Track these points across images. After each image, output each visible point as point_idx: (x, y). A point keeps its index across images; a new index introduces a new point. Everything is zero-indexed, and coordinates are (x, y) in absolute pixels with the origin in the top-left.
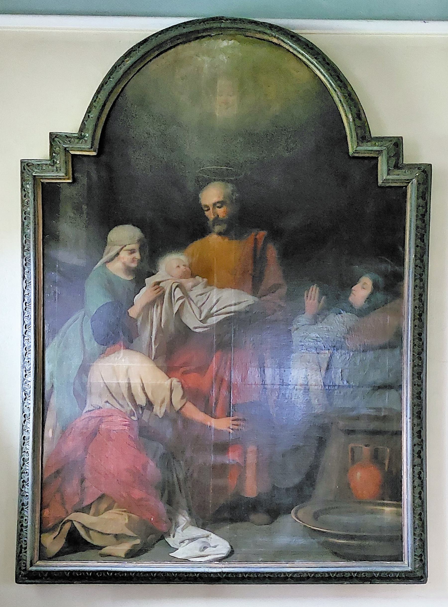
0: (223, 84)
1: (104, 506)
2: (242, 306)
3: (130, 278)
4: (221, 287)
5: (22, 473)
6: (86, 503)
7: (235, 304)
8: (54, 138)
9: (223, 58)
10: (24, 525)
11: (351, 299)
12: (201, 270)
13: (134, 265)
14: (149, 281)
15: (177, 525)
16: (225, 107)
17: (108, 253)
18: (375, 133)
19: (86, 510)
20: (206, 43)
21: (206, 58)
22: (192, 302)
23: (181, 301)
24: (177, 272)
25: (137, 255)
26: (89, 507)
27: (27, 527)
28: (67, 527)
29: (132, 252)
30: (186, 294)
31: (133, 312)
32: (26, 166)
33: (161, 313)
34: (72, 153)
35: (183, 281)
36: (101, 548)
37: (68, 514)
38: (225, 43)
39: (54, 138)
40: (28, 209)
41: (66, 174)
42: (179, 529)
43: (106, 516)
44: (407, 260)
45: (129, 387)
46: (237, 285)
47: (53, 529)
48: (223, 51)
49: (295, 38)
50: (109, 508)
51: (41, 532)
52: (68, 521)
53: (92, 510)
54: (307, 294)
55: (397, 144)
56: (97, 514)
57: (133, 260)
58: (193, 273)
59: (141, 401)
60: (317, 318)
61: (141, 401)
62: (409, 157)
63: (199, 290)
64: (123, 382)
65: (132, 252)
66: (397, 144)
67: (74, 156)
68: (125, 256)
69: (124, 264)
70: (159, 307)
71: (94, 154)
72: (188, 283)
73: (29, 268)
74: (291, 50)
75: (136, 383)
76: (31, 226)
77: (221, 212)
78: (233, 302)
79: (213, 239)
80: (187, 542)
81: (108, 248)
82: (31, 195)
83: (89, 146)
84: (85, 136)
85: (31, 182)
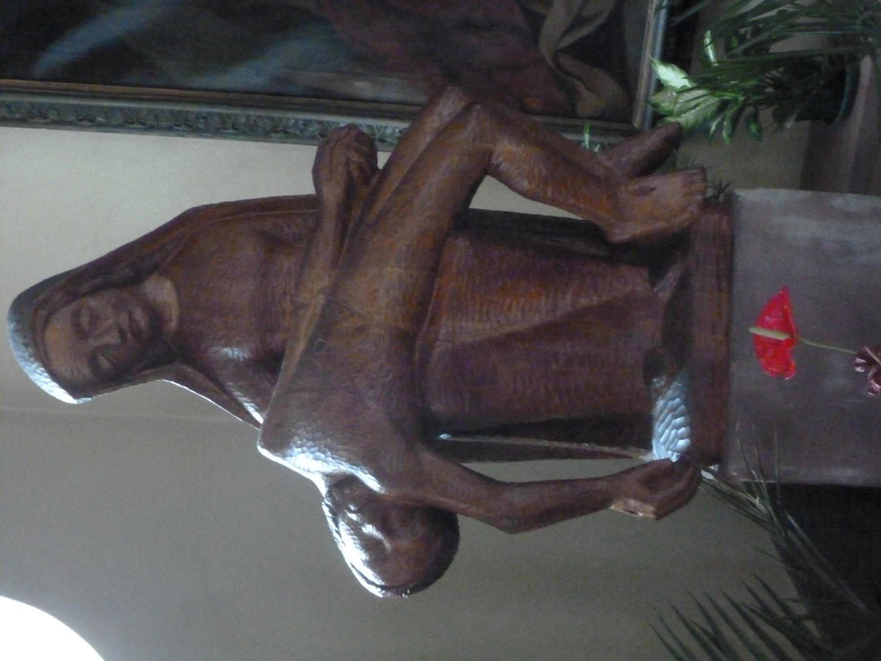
6: (519, 19)
28: (568, 63)
47: (572, 95)
52: (555, 59)
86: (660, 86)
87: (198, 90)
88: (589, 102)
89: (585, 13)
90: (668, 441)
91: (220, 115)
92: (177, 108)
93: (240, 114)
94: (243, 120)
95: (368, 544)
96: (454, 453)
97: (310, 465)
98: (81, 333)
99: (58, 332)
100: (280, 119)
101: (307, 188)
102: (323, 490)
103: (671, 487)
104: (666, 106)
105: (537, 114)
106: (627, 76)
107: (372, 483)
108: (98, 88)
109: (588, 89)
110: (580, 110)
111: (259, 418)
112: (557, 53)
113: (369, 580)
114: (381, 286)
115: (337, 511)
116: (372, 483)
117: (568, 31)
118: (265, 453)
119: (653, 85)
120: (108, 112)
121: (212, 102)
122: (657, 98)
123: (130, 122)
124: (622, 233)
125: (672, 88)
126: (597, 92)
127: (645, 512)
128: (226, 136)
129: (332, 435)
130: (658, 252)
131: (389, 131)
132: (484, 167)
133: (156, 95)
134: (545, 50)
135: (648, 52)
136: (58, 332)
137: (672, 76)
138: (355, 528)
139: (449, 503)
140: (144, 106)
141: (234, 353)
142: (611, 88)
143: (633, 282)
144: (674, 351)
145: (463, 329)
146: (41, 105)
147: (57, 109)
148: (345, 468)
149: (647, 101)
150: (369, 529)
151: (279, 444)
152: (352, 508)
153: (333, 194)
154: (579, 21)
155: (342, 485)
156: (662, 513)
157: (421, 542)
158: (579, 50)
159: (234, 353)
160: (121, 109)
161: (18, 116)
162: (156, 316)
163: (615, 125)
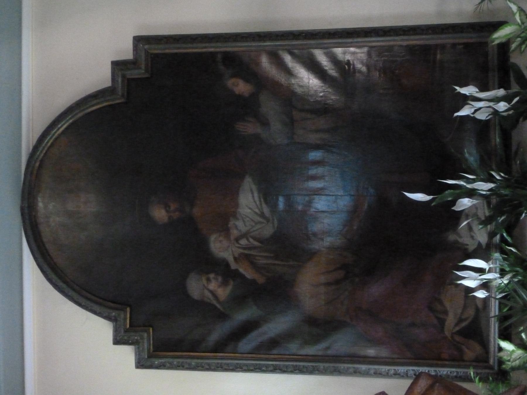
0: (71, 206)
1: (439, 307)
2: (254, 187)
3: (232, 282)
4: (237, 205)
5: (407, 375)
6: (435, 321)
7: (252, 193)
8: (117, 342)
9: (51, 206)
10: (455, 374)
11: (246, 94)
12: (223, 221)
13: (220, 279)
14: (233, 266)
15: (456, 242)
16: (88, 204)
17: (210, 299)
18: (109, 84)
19: (442, 322)
20: (41, 219)
21: (51, 220)
22: (251, 230)
23: (251, 240)
24: (225, 243)
25: (212, 276)
26: (438, 319)
27: (457, 372)
28: (458, 338)
29: (208, 280)
30: (245, 235)
31: (261, 280)
32: (140, 364)
33: (260, 256)
34: (128, 326)
35: (232, 238)
36: (477, 309)
37: (445, 338)
38: (41, 205)
39: (117, 342)
40: (175, 363)
41: (146, 331)
42: (460, 240)
43: (447, 304)
44: (212, 50)
45: (328, 284)
46: (234, 194)
47: (460, 351)
48: (46, 207)
49: (36, 148)
50: (441, 303)
51: (464, 361)
52: (452, 337)
53: (441, 316)
54: (243, 132)
55: (117, 65)
56: (446, 313)
57: (216, 279)
58: (225, 231)
59: (340, 274)
60: (265, 123)
61: (340, 274)
62: (129, 55)
63: (240, 224)
64: (322, 289)
65: (208, 280)
66: (117, 65)
67: (130, 326)
68: (213, 286)
69: (219, 286)
70: (257, 258)
71: (128, 309)
72: (235, 233)
73: (225, 364)
74: (44, 152)
75: (323, 279)
76: (189, 361)
77: (173, 206)
78: (250, 195)
79: (197, 211)
80: (472, 234)
81: (206, 300)
82: (163, 361)
83: (122, 312)
84: (115, 317)
85: (153, 360)
86: (500, 349)
87: (300, 355)
88: (469, 354)
89: (463, 317)
91: (313, 366)
92: (295, 363)
93: (321, 365)
94: (322, 367)
100: (338, 367)
104: (505, 358)
105: (446, 360)
106: (485, 344)
108: (262, 356)
109: (468, 349)
110: (466, 358)
112: (453, 334)
117: (457, 324)
119: (497, 349)
120: (267, 366)
121: (310, 361)
122: (501, 354)
123: (275, 370)
125: (508, 351)
126: (472, 350)
128: (315, 374)
131: (383, 370)
133: (287, 358)
134: (447, 333)
135: (492, 335)
137: (506, 345)
140: (281, 363)
142: (478, 349)
146: (241, 364)
147: (247, 365)
149: (494, 356)
154: (461, 321)
158: (460, 333)
160: (272, 365)
161: (231, 368)
163: (481, 364)
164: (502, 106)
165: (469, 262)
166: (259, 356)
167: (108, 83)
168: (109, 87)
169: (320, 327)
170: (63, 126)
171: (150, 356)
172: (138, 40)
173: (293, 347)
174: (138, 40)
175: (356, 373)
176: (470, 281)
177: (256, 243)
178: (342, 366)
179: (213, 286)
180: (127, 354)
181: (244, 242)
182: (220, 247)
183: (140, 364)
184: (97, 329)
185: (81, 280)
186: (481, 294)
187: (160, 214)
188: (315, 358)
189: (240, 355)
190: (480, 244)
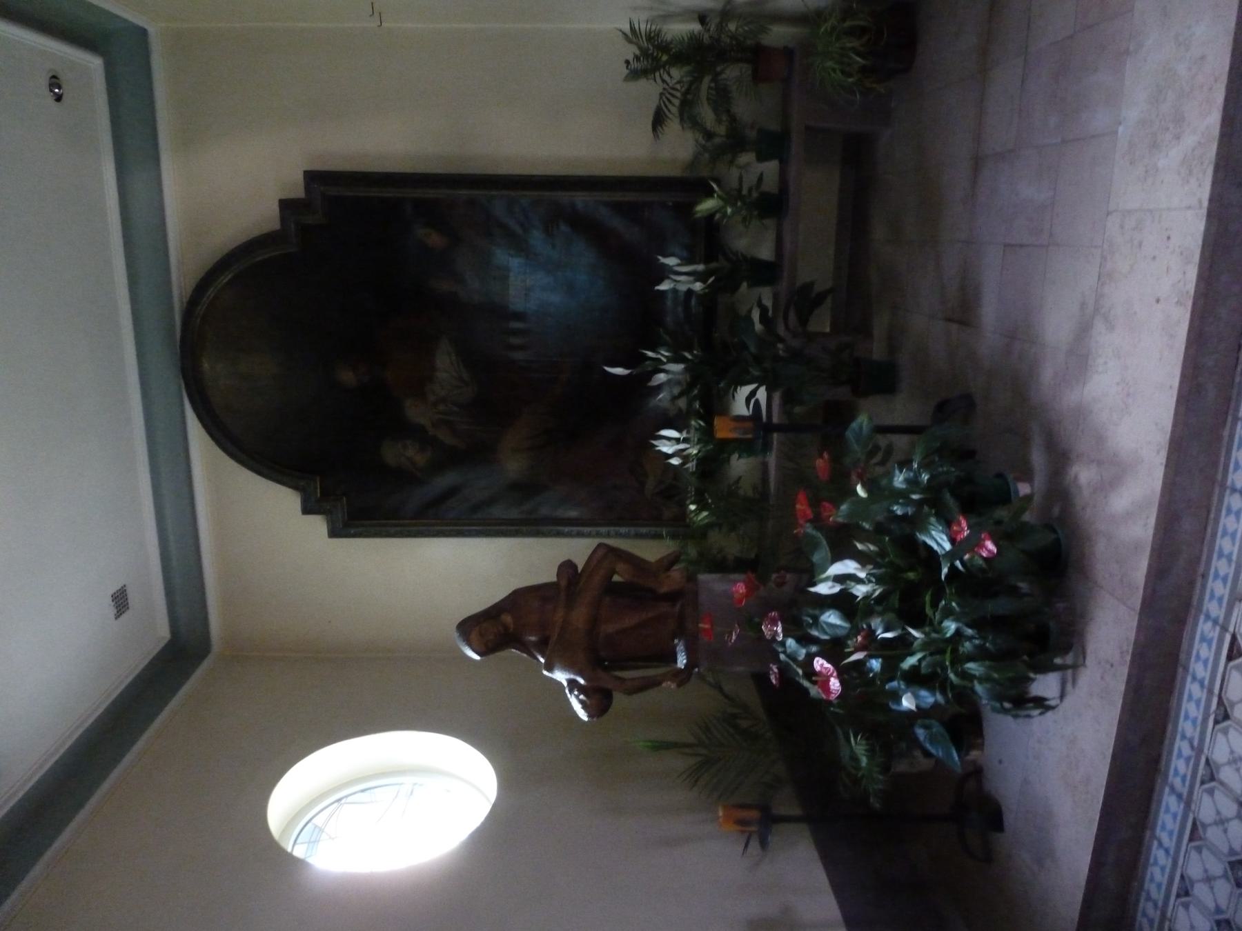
8: (307, 510)
32: (333, 533)
38: (206, 366)
39: (307, 510)
55: (285, 205)
62: (299, 193)
90: (682, 661)
93: (524, 529)
95: (581, 702)
96: (606, 669)
97: (561, 676)
98: (481, 635)
99: (474, 636)
101: (554, 579)
102: (565, 684)
103: (683, 677)
107: (582, 681)
111: (542, 660)
113: (583, 715)
114: (580, 616)
115: (571, 692)
116: (582, 681)
118: (545, 673)
124: (664, 589)
127: (673, 686)
129: (568, 666)
130: (672, 597)
132: (614, 572)
136: (474, 636)
138: (577, 697)
139: (610, 687)
141: (533, 638)
143: (664, 608)
144: (680, 632)
145: (609, 628)
148: (572, 676)
150: (582, 697)
151: (550, 669)
152: (671, 261)
153: (563, 583)
155: (572, 684)
156: (679, 686)
157: (599, 700)
159: (533, 638)
162: (506, 628)
164: (698, 286)
165: (665, 433)
166: (1204, 558)
167: (275, 225)
168: (277, 231)
169: (524, 489)
170: (226, 278)
171: (346, 525)
172: (312, 177)
173: (497, 511)
174: (312, 177)
175: (559, 534)
176: (667, 448)
177: (455, 409)
178: (545, 529)
179: (410, 452)
180: (318, 525)
181: (441, 407)
182: (416, 413)
183: (333, 533)
184: (285, 500)
185: (263, 449)
186: (675, 461)
187: (347, 377)
188: (511, 522)
189: (1221, 669)
190: (680, 410)
